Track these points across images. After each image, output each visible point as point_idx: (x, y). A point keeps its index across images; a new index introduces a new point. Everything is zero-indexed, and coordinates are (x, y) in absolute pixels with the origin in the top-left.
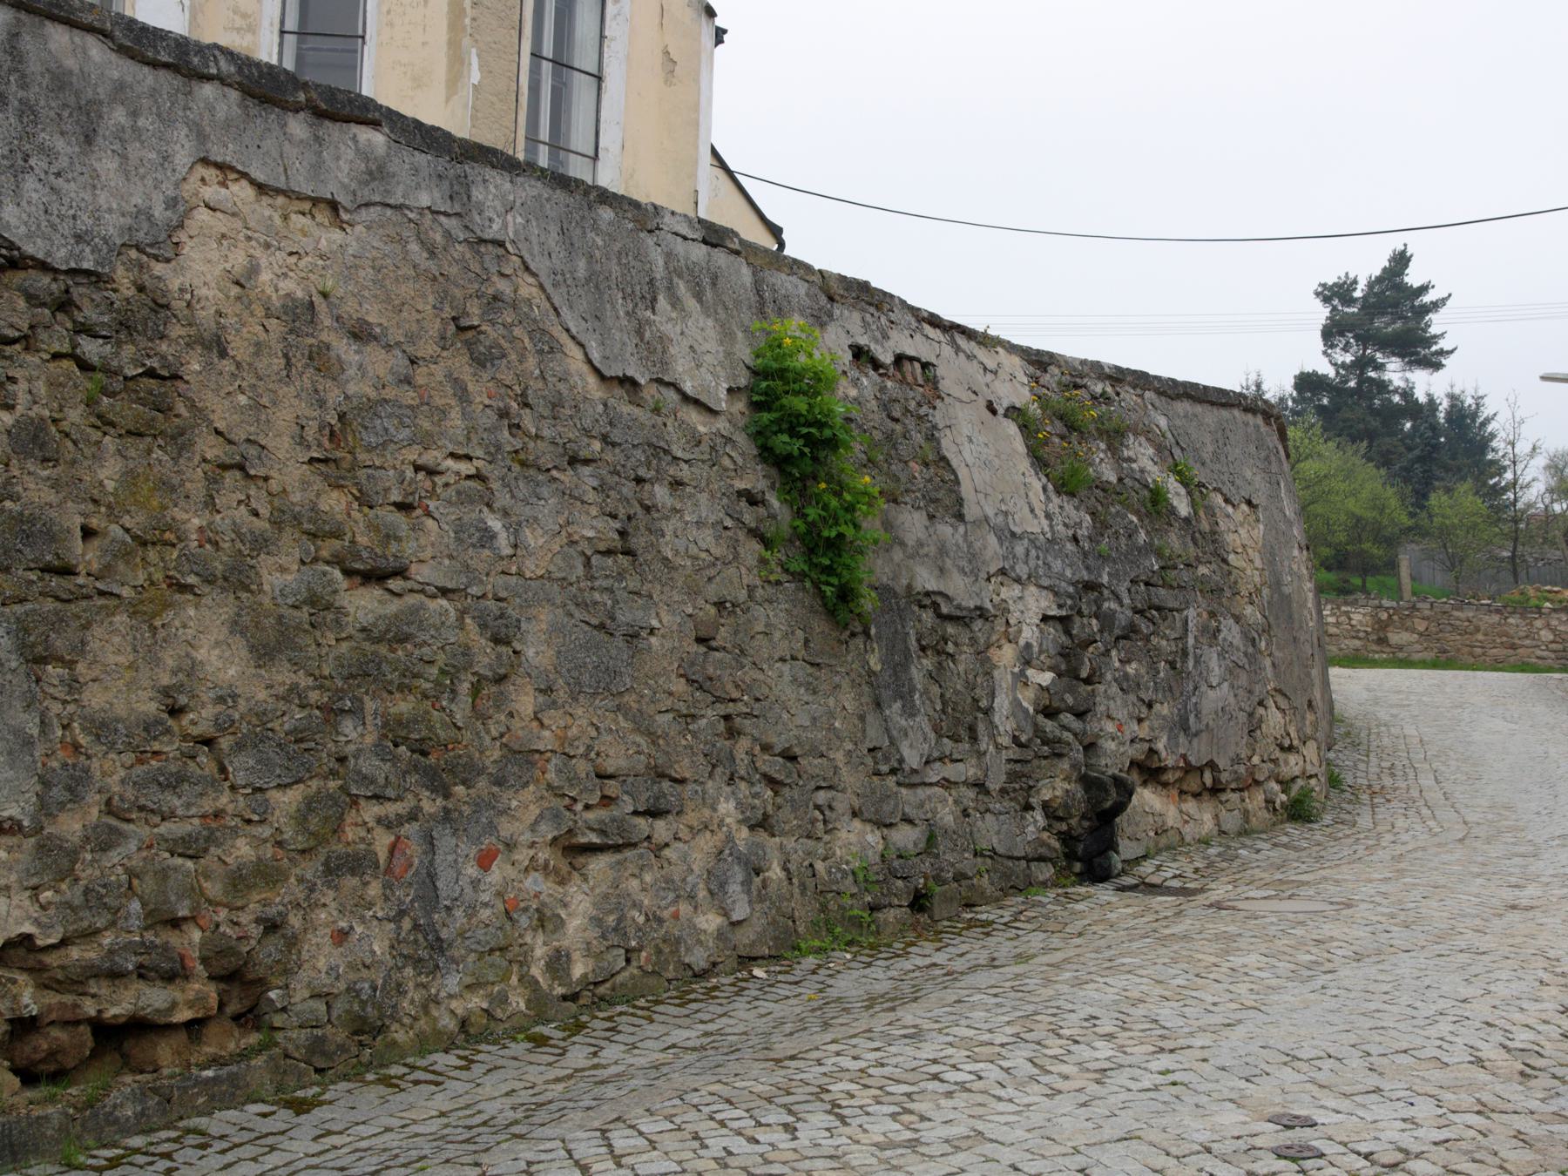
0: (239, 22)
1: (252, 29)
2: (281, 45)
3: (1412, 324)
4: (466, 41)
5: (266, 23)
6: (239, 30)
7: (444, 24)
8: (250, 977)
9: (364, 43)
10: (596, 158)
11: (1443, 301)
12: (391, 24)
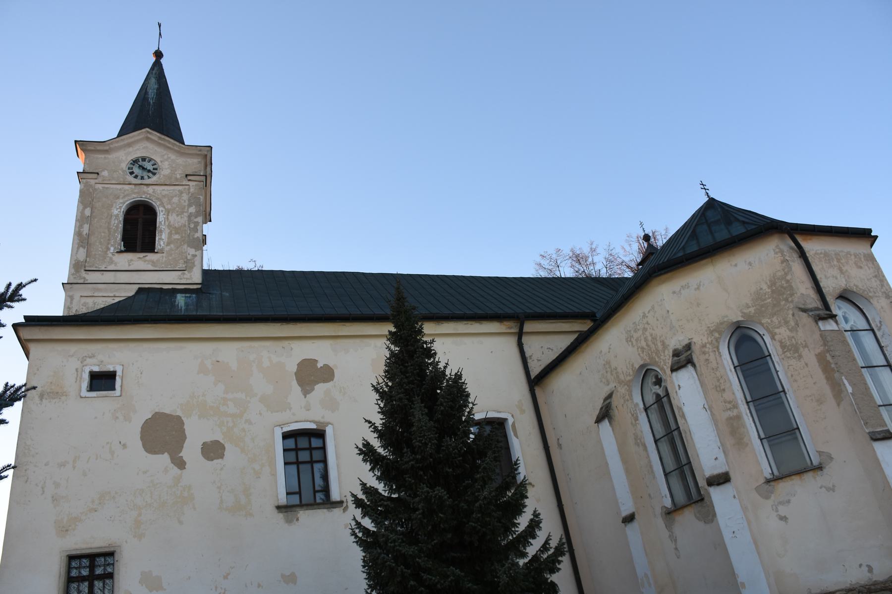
0: (729, 406)
1: (736, 406)
2: (749, 408)
4: (836, 375)
5: (740, 402)
6: (730, 409)
8: (196, 160)
12: (795, 381)
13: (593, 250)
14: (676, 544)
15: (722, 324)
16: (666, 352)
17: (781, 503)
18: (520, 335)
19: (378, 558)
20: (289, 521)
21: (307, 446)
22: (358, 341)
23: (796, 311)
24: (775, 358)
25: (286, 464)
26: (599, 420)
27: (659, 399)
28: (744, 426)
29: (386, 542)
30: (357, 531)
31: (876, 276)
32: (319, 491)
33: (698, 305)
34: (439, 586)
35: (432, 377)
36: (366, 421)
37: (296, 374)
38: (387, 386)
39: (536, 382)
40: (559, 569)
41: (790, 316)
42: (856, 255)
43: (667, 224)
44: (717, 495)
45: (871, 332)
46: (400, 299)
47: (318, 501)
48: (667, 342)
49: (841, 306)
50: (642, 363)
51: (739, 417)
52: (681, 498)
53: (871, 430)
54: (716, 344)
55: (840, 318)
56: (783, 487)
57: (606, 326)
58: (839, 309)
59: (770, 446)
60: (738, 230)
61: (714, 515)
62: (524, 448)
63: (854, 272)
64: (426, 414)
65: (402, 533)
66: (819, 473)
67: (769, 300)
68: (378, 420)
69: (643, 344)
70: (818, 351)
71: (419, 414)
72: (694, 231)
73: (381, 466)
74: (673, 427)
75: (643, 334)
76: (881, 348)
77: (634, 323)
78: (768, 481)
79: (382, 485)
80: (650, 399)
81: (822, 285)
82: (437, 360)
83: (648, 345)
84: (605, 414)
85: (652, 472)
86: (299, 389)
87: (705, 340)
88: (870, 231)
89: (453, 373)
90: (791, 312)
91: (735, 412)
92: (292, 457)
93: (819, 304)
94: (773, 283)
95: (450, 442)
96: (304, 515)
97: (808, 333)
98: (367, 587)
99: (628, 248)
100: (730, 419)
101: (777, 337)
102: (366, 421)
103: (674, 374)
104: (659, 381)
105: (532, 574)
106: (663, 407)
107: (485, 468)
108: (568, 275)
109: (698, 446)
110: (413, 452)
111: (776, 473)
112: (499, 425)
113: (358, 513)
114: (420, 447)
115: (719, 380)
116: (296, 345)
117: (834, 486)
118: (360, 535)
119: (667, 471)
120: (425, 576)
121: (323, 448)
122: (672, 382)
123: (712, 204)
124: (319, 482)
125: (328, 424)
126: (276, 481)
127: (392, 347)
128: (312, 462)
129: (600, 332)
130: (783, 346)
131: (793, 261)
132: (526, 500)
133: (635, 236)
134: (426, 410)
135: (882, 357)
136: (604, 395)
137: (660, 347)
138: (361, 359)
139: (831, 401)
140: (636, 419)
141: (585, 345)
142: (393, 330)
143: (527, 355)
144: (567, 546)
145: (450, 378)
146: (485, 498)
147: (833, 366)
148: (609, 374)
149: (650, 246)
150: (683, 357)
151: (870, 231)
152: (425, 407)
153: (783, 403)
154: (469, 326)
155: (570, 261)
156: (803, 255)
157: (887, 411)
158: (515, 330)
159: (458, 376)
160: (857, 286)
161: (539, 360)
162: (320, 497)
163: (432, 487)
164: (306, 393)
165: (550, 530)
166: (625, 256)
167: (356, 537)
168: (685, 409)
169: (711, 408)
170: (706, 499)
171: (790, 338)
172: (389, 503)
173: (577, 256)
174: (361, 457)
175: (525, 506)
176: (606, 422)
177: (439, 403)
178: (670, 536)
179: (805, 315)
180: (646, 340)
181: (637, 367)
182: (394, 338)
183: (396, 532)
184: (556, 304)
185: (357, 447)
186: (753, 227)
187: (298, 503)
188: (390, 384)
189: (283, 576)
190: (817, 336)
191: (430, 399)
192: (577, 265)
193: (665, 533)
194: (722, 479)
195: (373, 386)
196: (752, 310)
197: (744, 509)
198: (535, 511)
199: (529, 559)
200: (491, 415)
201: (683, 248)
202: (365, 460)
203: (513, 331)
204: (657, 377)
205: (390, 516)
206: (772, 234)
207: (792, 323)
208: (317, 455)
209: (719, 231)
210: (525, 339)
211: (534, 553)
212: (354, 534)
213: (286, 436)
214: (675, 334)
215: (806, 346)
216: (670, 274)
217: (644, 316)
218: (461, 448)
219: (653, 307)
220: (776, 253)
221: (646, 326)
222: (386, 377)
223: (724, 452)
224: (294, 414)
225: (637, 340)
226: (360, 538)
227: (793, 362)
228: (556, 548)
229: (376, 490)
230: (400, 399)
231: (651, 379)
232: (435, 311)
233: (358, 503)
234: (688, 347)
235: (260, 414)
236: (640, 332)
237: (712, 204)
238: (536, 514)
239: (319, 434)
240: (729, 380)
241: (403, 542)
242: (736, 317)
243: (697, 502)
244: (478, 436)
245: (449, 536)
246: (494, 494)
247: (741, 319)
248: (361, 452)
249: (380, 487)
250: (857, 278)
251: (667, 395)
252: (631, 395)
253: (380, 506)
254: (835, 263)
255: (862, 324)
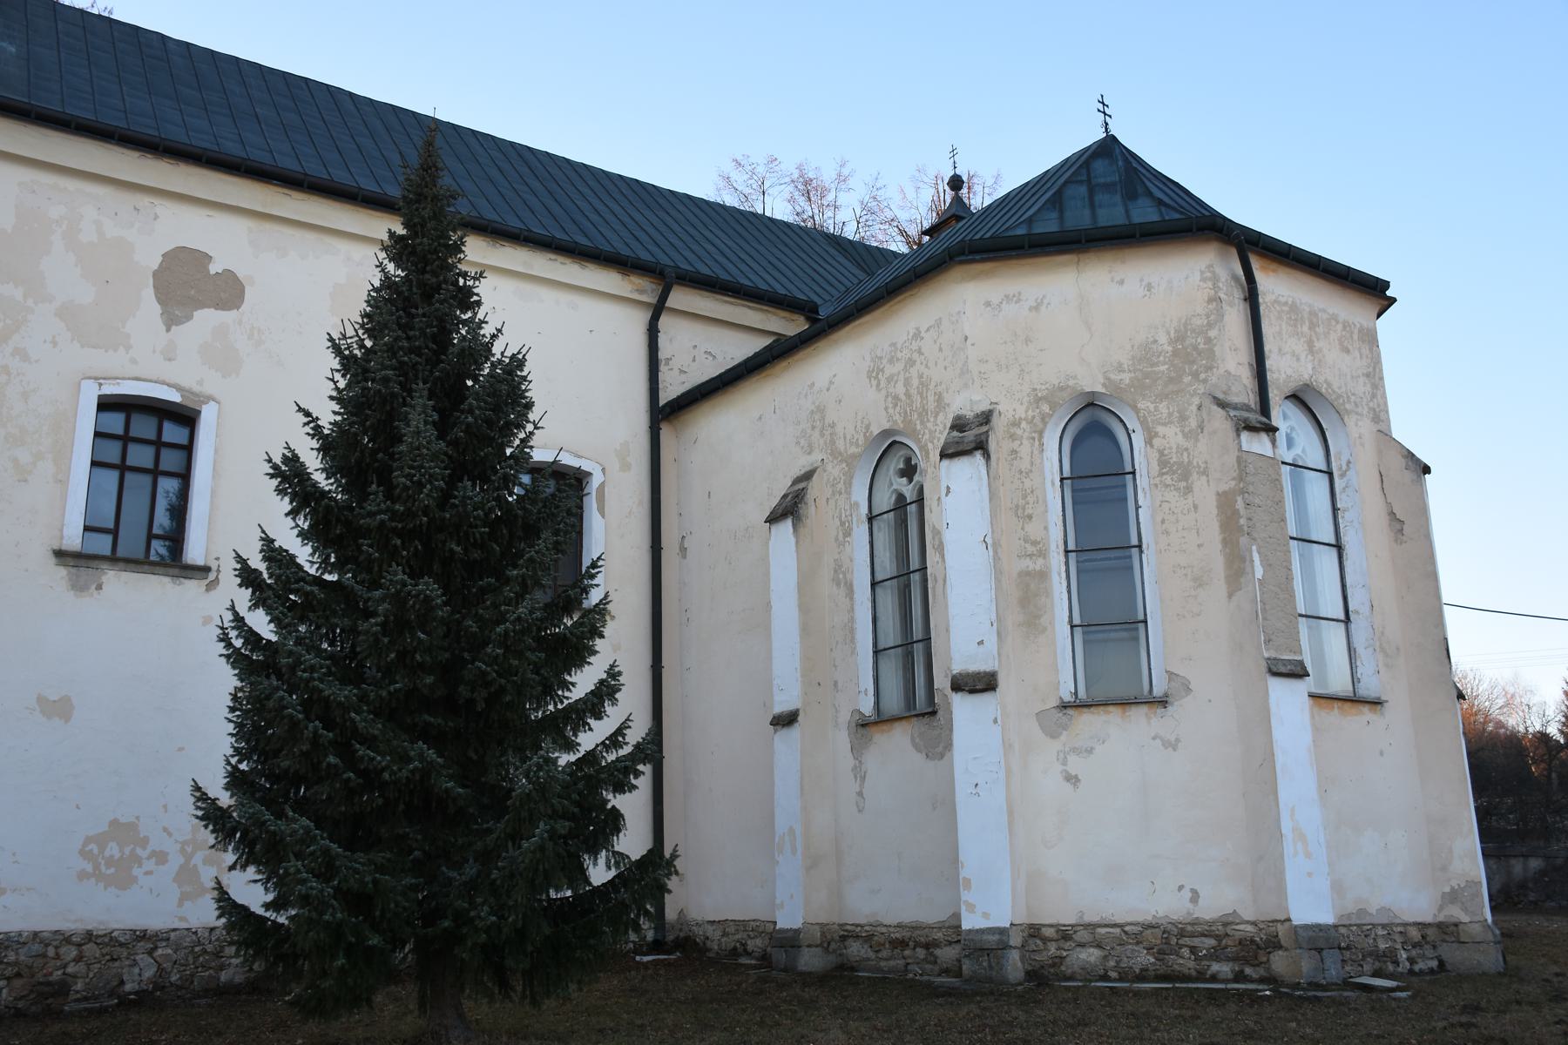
0: (1030, 549)
1: (1043, 554)
2: (1067, 563)
3: (470, 283)
4: (1244, 540)
5: (1053, 547)
6: (1031, 556)
7: (1215, 526)
9: (1141, 552)
10: (1347, 620)
11: (675, 850)
12: (1167, 533)
13: (841, 179)
14: (862, 786)
15: (1061, 389)
16: (941, 417)
17: (1074, 750)
18: (658, 310)
19: (268, 698)
20: (78, 587)
21: (152, 436)
22: (298, 234)
23: (1208, 402)
24: (1142, 481)
25: (95, 464)
26: (773, 519)
27: (901, 504)
28: (1048, 593)
29: (293, 668)
30: (233, 634)
31: (1368, 375)
32: (158, 537)
33: (1028, 341)
34: (386, 776)
35: (463, 350)
36: (300, 409)
37: (155, 274)
38: (362, 346)
39: (667, 413)
40: (635, 787)
41: (1194, 408)
42: (1346, 325)
43: (1004, 167)
44: (963, 709)
45: (1325, 477)
46: (430, 168)
47: (153, 558)
48: (947, 398)
49: (1289, 413)
50: (887, 426)
51: (1043, 575)
52: (893, 700)
53: (1273, 654)
54: (1041, 426)
55: (1281, 436)
56: (1089, 722)
57: (835, 336)
58: (1285, 417)
59: (1085, 642)
60: (1145, 213)
61: (949, 746)
62: (611, 536)
63: (1332, 354)
64: (434, 423)
65: (331, 657)
66: (1160, 711)
67: (1163, 368)
68: (328, 414)
69: (900, 389)
70: (1224, 487)
71: (418, 419)
72: (1059, 193)
73: (314, 512)
74: (915, 563)
75: (905, 369)
76: (1335, 510)
77: (894, 345)
78: (1064, 706)
79: (309, 549)
80: (885, 501)
81: (1268, 363)
82: (480, 316)
83: (907, 394)
84: (789, 509)
85: (853, 640)
86: (158, 309)
87: (1021, 413)
88: (1386, 285)
89: (508, 353)
90: (1196, 401)
91: (1039, 564)
92: (112, 452)
93: (1252, 399)
94: (1180, 337)
95: (470, 490)
96: (119, 585)
97: (1218, 448)
98: (230, 751)
99: (911, 194)
100: (1026, 574)
101: (1156, 442)
102: (300, 409)
103: (946, 462)
104: (909, 471)
105: (581, 785)
106: (905, 520)
107: (531, 560)
108: (778, 216)
109: (954, 610)
110: (389, 496)
111: (1082, 694)
112: (570, 482)
113: (243, 597)
114: (406, 488)
115: (1024, 497)
116: (168, 211)
117: (1178, 740)
118: (238, 643)
119: (881, 646)
120: (361, 751)
121: (188, 449)
122: (937, 479)
123: (1109, 147)
124: (162, 519)
125: (209, 399)
126: (68, 496)
127: (391, 267)
128: (155, 473)
129: (821, 344)
130: (1163, 463)
131: (1231, 305)
132: (598, 641)
133: (932, 173)
134: (436, 417)
135: (1331, 528)
136: (797, 471)
137: (931, 405)
138: (314, 278)
139: (1219, 585)
140: (848, 533)
141: (784, 364)
142: (400, 230)
143: (662, 355)
144: (652, 750)
145: (500, 361)
146: (519, 619)
147: (1242, 521)
148: (816, 433)
149: (957, 200)
150: (970, 435)
151: (1386, 285)
152: (434, 409)
153: (1131, 568)
154: (557, 265)
155: (791, 188)
156: (1252, 297)
157: (1309, 627)
158: (651, 299)
159: (518, 362)
160: (1329, 385)
161: (682, 372)
162: (159, 547)
163: (415, 575)
164: (171, 321)
165: (629, 709)
166: (902, 208)
167: (229, 645)
168: (948, 537)
169: (996, 545)
170: (940, 713)
171: (1181, 450)
172: (315, 589)
173: (807, 182)
174: (275, 482)
175: (595, 653)
176: (787, 525)
177: (465, 406)
178: (854, 769)
179: (1220, 412)
180: (907, 382)
181: (876, 432)
182: (398, 249)
183: (319, 652)
184: (743, 267)
185: (270, 461)
186: (1177, 216)
187: (108, 552)
188: (368, 343)
189: (41, 700)
190: (1234, 454)
191: (449, 396)
192: (802, 201)
193: (847, 761)
194: (981, 684)
195: (331, 339)
196: (1126, 377)
197: (1007, 747)
198: (612, 666)
199: (579, 755)
200: (567, 460)
201: (1030, 221)
202: (280, 491)
203: (644, 298)
204: (908, 460)
205: (311, 615)
206: (1208, 240)
207: (1193, 423)
208: (170, 460)
209: (1108, 205)
210: (665, 322)
211: (591, 747)
212: (225, 639)
213: (106, 405)
214: (966, 386)
215: (1205, 473)
216: (988, 266)
217: (917, 335)
218: (491, 510)
219: (939, 322)
220: (1203, 280)
221: (916, 356)
222: (362, 326)
223: (999, 634)
224: (134, 361)
225: (889, 380)
226: (237, 650)
227: (1172, 496)
228: (637, 746)
229: (293, 557)
230: (386, 380)
231: (896, 462)
232: (490, 215)
233: (248, 577)
234: (986, 418)
235: (55, 344)
236: (899, 366)
237: (1109, 147)
238: (613, 673)
239: (187, 418)
240: (1045, 502)
241: (329, 673)
242: (1093, 383)
243: (923, 715)
244: (531, 494)
245: (429, 680)
246: (538, 614)
247: (1100, 389)
248: (276, 472)
249: (304, 554)
250: (1333, 370)
251: (920, 500)
252: (849, 484)
253: (295, 592)
254: (1305, 329)
255: (1315, 458)
